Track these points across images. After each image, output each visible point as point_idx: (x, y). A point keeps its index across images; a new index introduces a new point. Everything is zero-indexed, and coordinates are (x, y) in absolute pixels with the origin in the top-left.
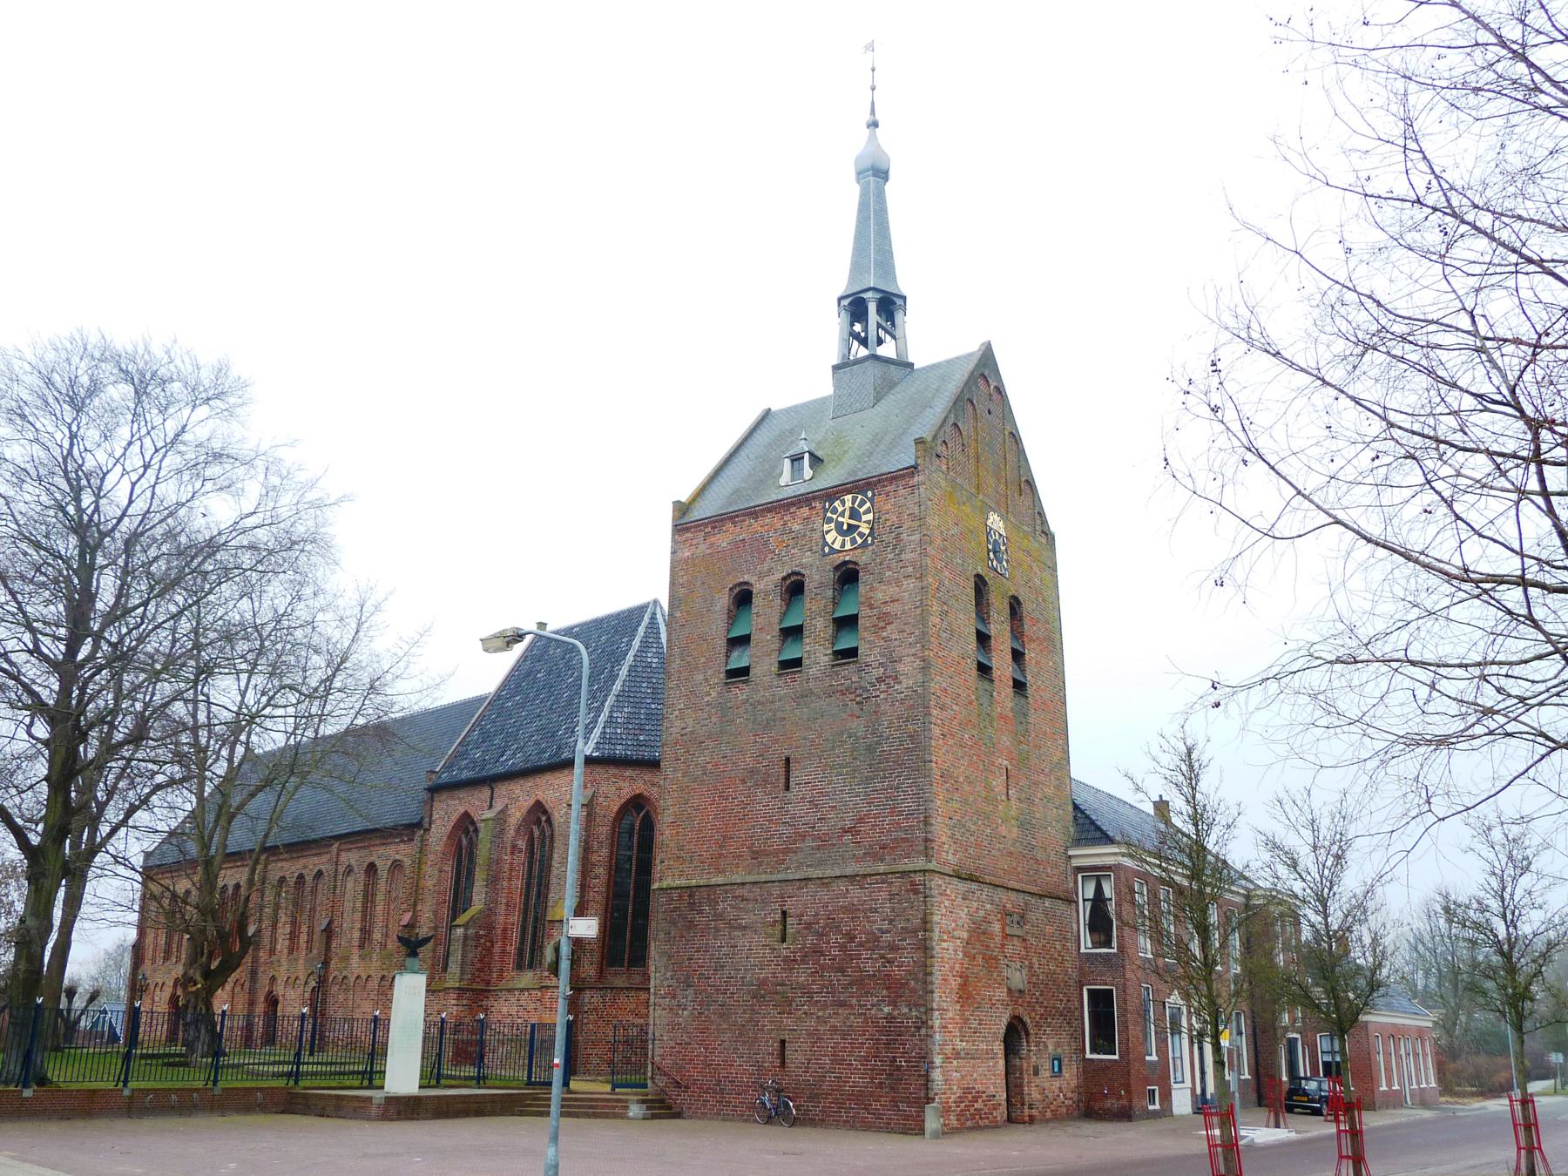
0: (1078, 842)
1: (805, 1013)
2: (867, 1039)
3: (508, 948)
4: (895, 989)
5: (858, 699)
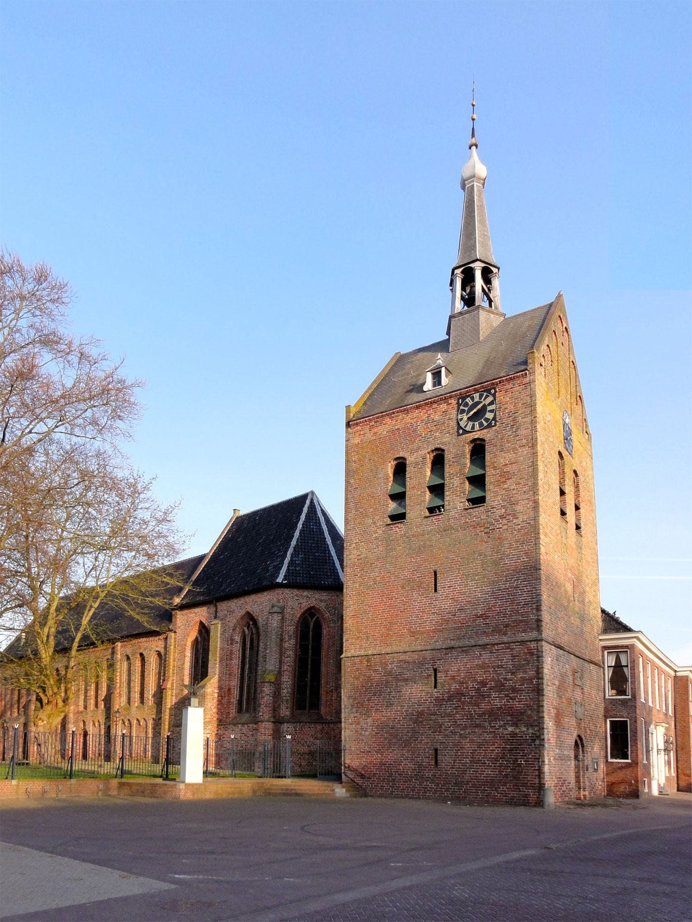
0: (605, 631)
1: (452, 732)
2: (496, 748)
3: (232, 700)
4: (517, 717)
5: (486, 530)
